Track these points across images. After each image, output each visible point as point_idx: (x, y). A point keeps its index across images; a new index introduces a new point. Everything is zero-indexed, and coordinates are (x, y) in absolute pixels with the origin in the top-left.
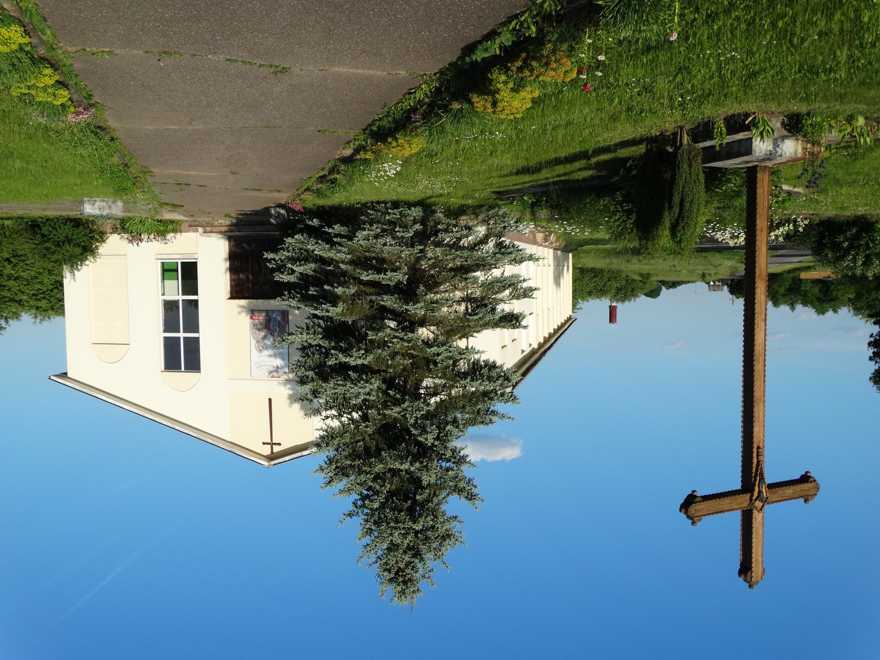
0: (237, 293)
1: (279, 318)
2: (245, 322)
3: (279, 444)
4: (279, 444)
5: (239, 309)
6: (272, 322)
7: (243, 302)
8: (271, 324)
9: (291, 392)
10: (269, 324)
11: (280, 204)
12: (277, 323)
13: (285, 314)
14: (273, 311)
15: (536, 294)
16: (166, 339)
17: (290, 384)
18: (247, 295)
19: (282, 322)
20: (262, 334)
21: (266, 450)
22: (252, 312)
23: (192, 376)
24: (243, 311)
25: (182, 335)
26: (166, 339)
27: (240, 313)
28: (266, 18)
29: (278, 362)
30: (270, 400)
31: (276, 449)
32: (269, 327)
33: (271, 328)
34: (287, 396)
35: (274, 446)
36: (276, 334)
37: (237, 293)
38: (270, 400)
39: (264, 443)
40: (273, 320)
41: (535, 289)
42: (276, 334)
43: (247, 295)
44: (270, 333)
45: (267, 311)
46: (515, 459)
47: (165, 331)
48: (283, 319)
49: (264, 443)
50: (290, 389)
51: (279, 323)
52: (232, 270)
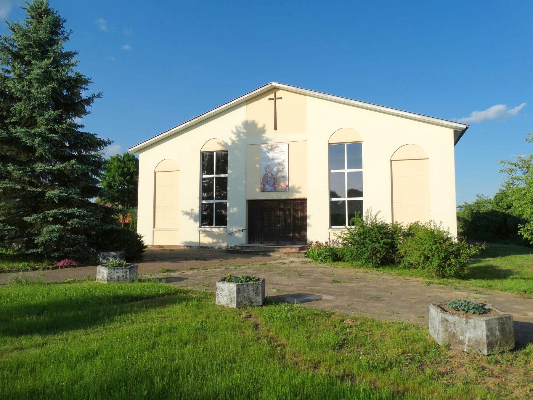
0: (303, 202)
1: (267, 186)
2: (293, 183)
3: (270, 99)
4: (270, 99)
5: (300, 190)
6: (272, 184)
7: (297, 196)
8: (273, 182)
9: (264, 135)
10: (274, 182)
11: (36, 271)
12: (268, 183)
13: (263, 190)
14: (271, 191)
15: (182, 210)
16: (361, 167)
17: (263, 140)
18: (288, 202)
19: (265, 183)
20: (279, 174)
21: (279, 94)
22: (287, 189)
23: (336, 140)
24: (297, 189)
25: (346, 171)
26: (361, 167)
27: (299, 188)
28: (463, 396)
29: (271, 155)
30: (276, 129)
31: (272, 96)
32: (274, 180)
33: (273, 180)
34: (267, 132)
35: (277, 97)
36: (269, 175)
37: (303, 202)
38: (276, 129)
39: (281, 98)
40: (272, 185)
41: (187, 214)
42: (269, 175)
43: (288, 202)
44: (273, 175)
45: (275, 191)
46: (483, 111)
47: (361, 172)
48: (264, 186)
49: (281, 98)
50: (264, 137)
51: (267, 183)
52: (304, 218)
